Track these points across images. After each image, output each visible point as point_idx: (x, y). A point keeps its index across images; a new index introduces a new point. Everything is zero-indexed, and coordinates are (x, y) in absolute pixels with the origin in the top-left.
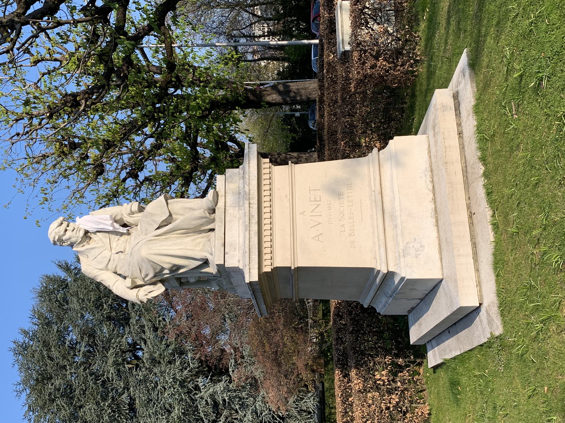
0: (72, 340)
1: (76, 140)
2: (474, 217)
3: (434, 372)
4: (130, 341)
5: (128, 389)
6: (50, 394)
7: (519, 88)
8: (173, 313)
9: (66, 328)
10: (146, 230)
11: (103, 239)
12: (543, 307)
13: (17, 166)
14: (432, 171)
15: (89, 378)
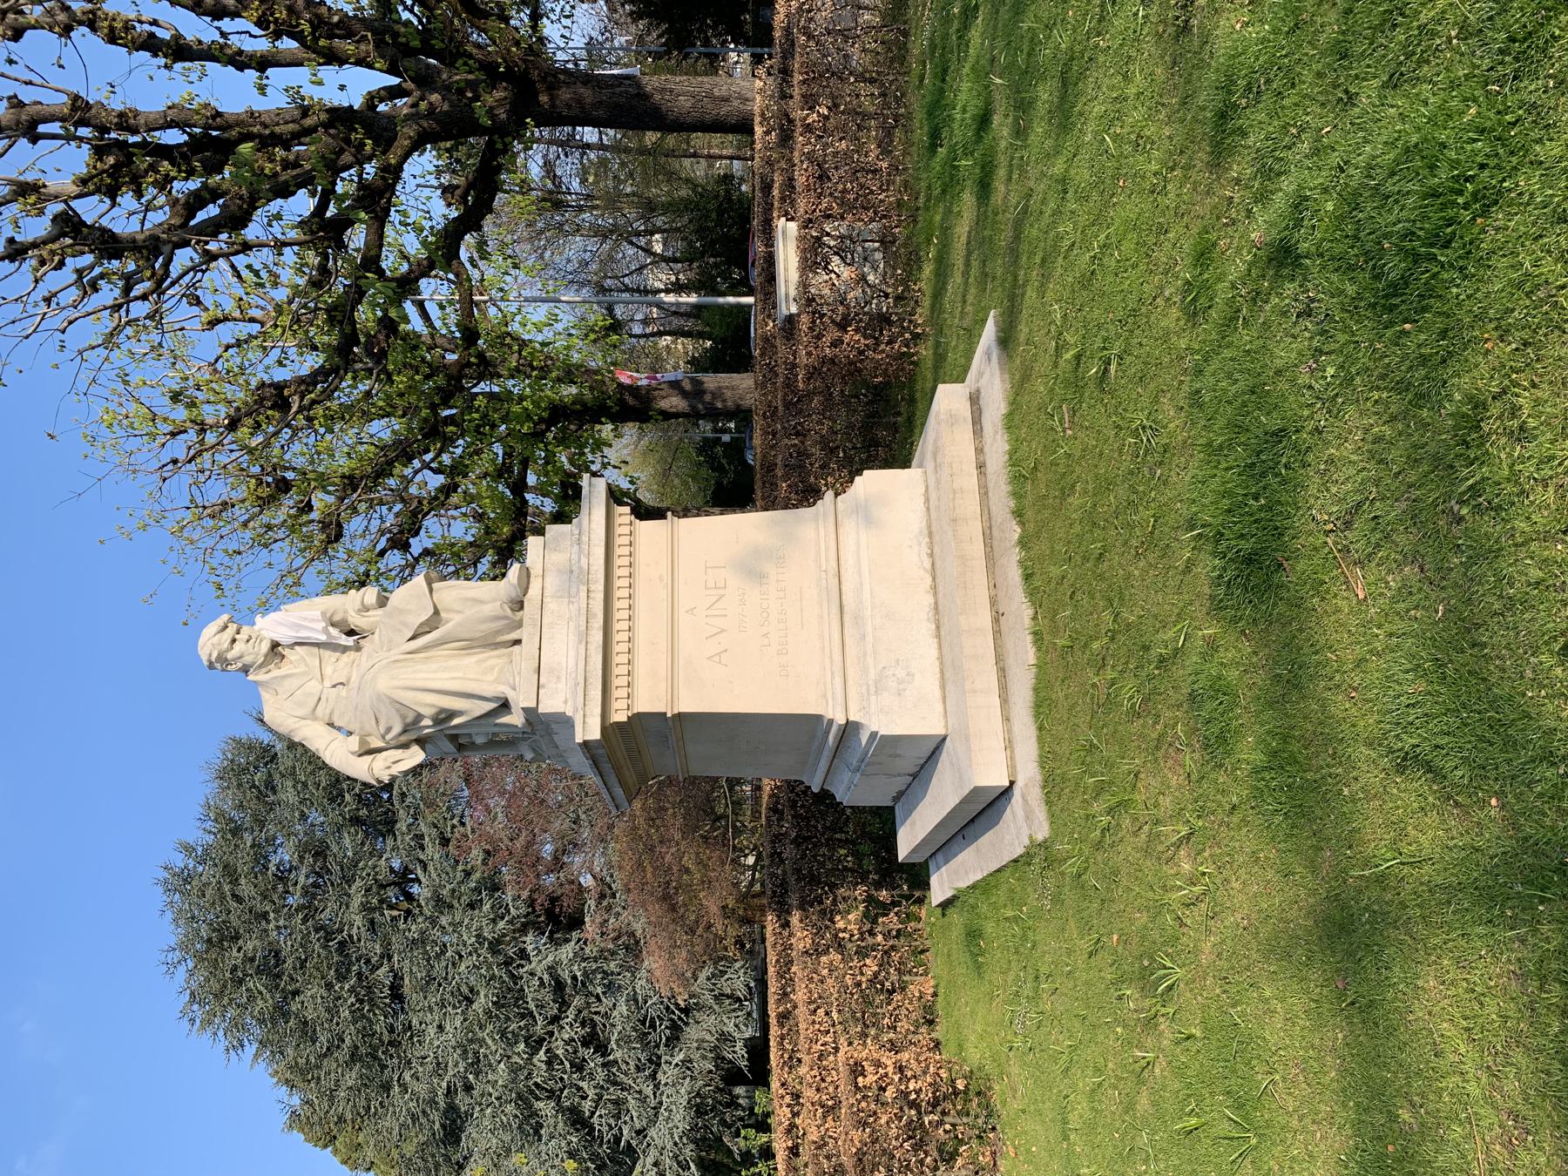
0: (281, 862)
1: (290, 475)
2: (1002, 619)
3: (944, 915)
4: (396, 864)
5: (390, 958)
6: (234, 969)
7: (1076, 383)
8: (479, 814)
9: (271, 840)
10: (390, 641)
12: (1111, 783)
13: (170, 524)
14: (930, 534)
15: (313, 937)
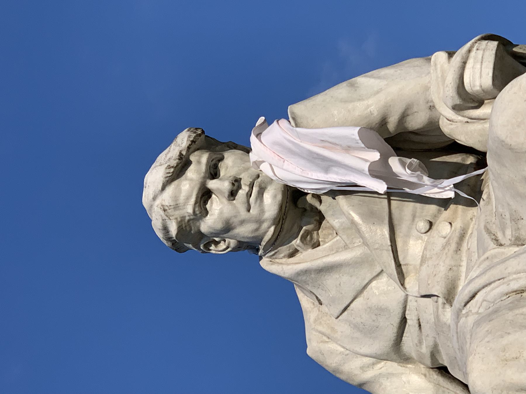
11: (364, 227)
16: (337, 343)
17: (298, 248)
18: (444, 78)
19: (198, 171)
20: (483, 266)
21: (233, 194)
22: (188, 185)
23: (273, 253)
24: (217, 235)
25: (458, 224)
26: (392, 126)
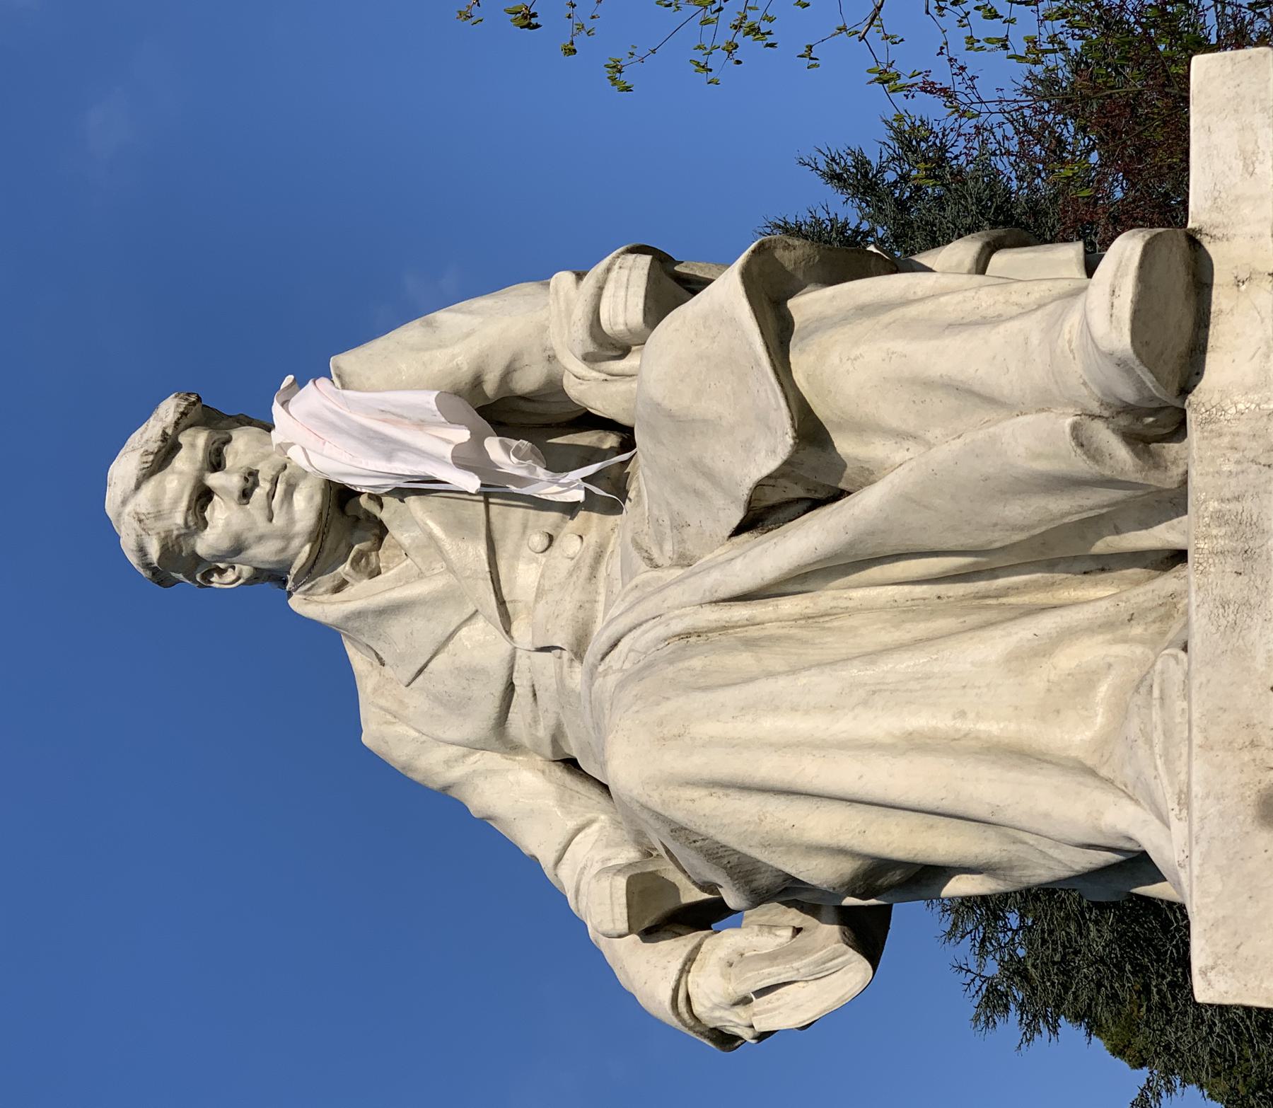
11: (447, 543)
16: (408, 725)
17: (347, 578)
18: (569, 314)
19: (191, 460)
20: (630, 599)
21: (246, 495)
22: (176, 481)
23: (308, 586)
24: (221, 558)
25: (592, 538)
26: (490, 387)
